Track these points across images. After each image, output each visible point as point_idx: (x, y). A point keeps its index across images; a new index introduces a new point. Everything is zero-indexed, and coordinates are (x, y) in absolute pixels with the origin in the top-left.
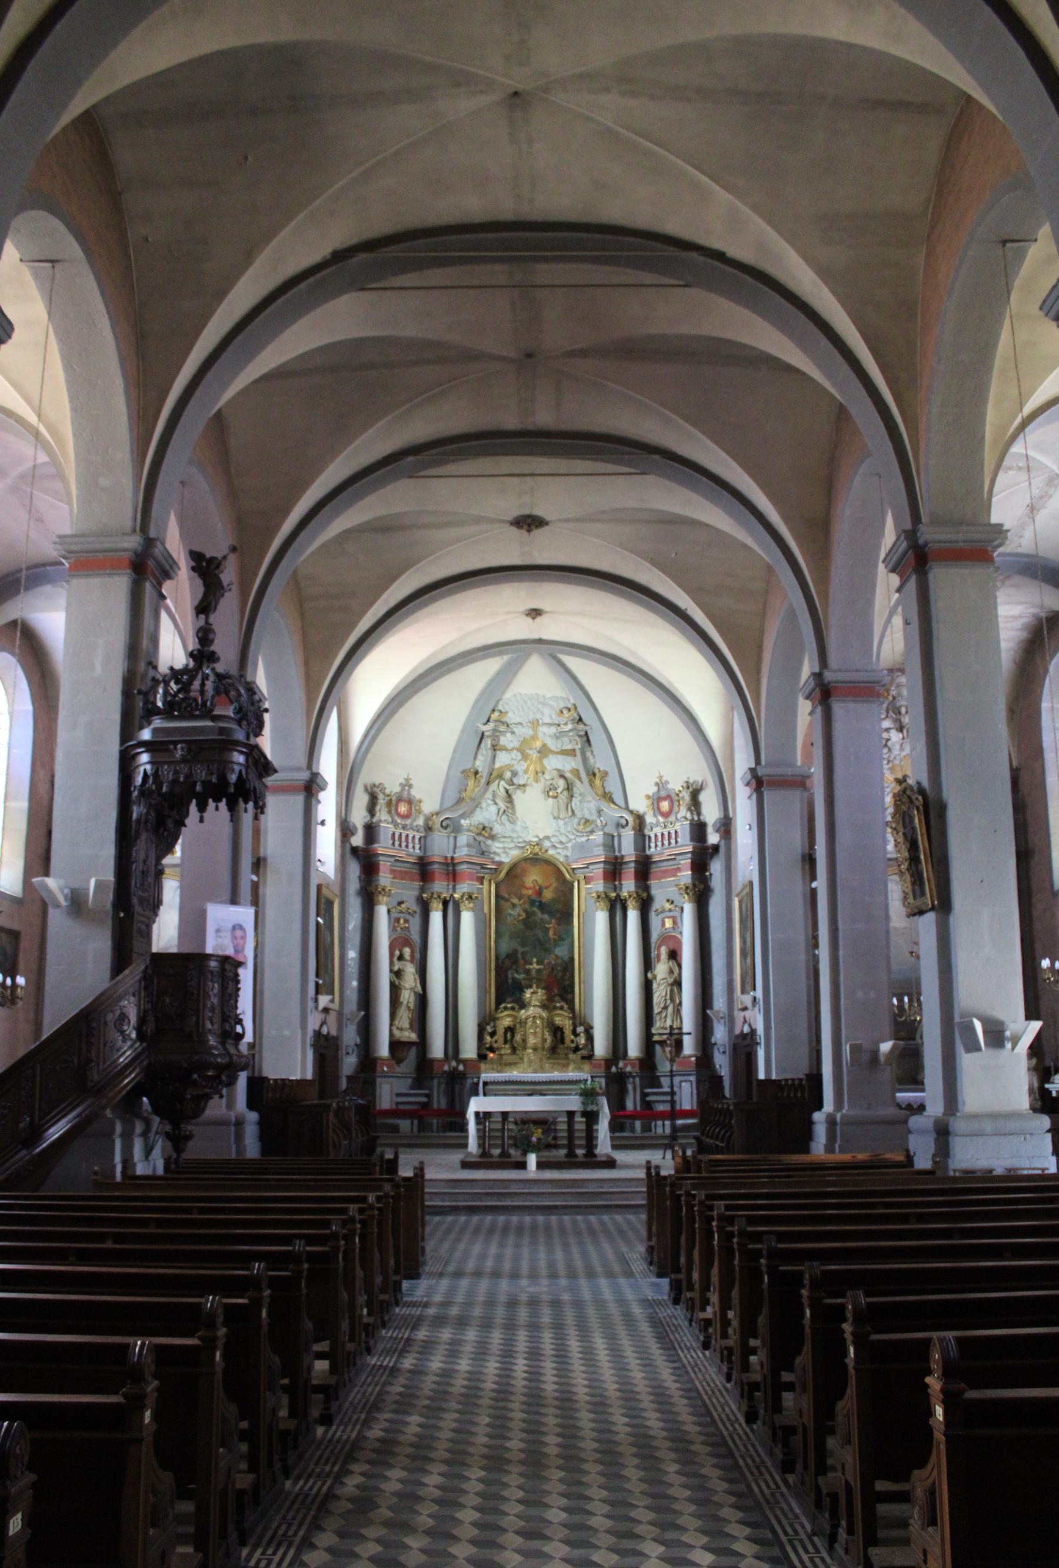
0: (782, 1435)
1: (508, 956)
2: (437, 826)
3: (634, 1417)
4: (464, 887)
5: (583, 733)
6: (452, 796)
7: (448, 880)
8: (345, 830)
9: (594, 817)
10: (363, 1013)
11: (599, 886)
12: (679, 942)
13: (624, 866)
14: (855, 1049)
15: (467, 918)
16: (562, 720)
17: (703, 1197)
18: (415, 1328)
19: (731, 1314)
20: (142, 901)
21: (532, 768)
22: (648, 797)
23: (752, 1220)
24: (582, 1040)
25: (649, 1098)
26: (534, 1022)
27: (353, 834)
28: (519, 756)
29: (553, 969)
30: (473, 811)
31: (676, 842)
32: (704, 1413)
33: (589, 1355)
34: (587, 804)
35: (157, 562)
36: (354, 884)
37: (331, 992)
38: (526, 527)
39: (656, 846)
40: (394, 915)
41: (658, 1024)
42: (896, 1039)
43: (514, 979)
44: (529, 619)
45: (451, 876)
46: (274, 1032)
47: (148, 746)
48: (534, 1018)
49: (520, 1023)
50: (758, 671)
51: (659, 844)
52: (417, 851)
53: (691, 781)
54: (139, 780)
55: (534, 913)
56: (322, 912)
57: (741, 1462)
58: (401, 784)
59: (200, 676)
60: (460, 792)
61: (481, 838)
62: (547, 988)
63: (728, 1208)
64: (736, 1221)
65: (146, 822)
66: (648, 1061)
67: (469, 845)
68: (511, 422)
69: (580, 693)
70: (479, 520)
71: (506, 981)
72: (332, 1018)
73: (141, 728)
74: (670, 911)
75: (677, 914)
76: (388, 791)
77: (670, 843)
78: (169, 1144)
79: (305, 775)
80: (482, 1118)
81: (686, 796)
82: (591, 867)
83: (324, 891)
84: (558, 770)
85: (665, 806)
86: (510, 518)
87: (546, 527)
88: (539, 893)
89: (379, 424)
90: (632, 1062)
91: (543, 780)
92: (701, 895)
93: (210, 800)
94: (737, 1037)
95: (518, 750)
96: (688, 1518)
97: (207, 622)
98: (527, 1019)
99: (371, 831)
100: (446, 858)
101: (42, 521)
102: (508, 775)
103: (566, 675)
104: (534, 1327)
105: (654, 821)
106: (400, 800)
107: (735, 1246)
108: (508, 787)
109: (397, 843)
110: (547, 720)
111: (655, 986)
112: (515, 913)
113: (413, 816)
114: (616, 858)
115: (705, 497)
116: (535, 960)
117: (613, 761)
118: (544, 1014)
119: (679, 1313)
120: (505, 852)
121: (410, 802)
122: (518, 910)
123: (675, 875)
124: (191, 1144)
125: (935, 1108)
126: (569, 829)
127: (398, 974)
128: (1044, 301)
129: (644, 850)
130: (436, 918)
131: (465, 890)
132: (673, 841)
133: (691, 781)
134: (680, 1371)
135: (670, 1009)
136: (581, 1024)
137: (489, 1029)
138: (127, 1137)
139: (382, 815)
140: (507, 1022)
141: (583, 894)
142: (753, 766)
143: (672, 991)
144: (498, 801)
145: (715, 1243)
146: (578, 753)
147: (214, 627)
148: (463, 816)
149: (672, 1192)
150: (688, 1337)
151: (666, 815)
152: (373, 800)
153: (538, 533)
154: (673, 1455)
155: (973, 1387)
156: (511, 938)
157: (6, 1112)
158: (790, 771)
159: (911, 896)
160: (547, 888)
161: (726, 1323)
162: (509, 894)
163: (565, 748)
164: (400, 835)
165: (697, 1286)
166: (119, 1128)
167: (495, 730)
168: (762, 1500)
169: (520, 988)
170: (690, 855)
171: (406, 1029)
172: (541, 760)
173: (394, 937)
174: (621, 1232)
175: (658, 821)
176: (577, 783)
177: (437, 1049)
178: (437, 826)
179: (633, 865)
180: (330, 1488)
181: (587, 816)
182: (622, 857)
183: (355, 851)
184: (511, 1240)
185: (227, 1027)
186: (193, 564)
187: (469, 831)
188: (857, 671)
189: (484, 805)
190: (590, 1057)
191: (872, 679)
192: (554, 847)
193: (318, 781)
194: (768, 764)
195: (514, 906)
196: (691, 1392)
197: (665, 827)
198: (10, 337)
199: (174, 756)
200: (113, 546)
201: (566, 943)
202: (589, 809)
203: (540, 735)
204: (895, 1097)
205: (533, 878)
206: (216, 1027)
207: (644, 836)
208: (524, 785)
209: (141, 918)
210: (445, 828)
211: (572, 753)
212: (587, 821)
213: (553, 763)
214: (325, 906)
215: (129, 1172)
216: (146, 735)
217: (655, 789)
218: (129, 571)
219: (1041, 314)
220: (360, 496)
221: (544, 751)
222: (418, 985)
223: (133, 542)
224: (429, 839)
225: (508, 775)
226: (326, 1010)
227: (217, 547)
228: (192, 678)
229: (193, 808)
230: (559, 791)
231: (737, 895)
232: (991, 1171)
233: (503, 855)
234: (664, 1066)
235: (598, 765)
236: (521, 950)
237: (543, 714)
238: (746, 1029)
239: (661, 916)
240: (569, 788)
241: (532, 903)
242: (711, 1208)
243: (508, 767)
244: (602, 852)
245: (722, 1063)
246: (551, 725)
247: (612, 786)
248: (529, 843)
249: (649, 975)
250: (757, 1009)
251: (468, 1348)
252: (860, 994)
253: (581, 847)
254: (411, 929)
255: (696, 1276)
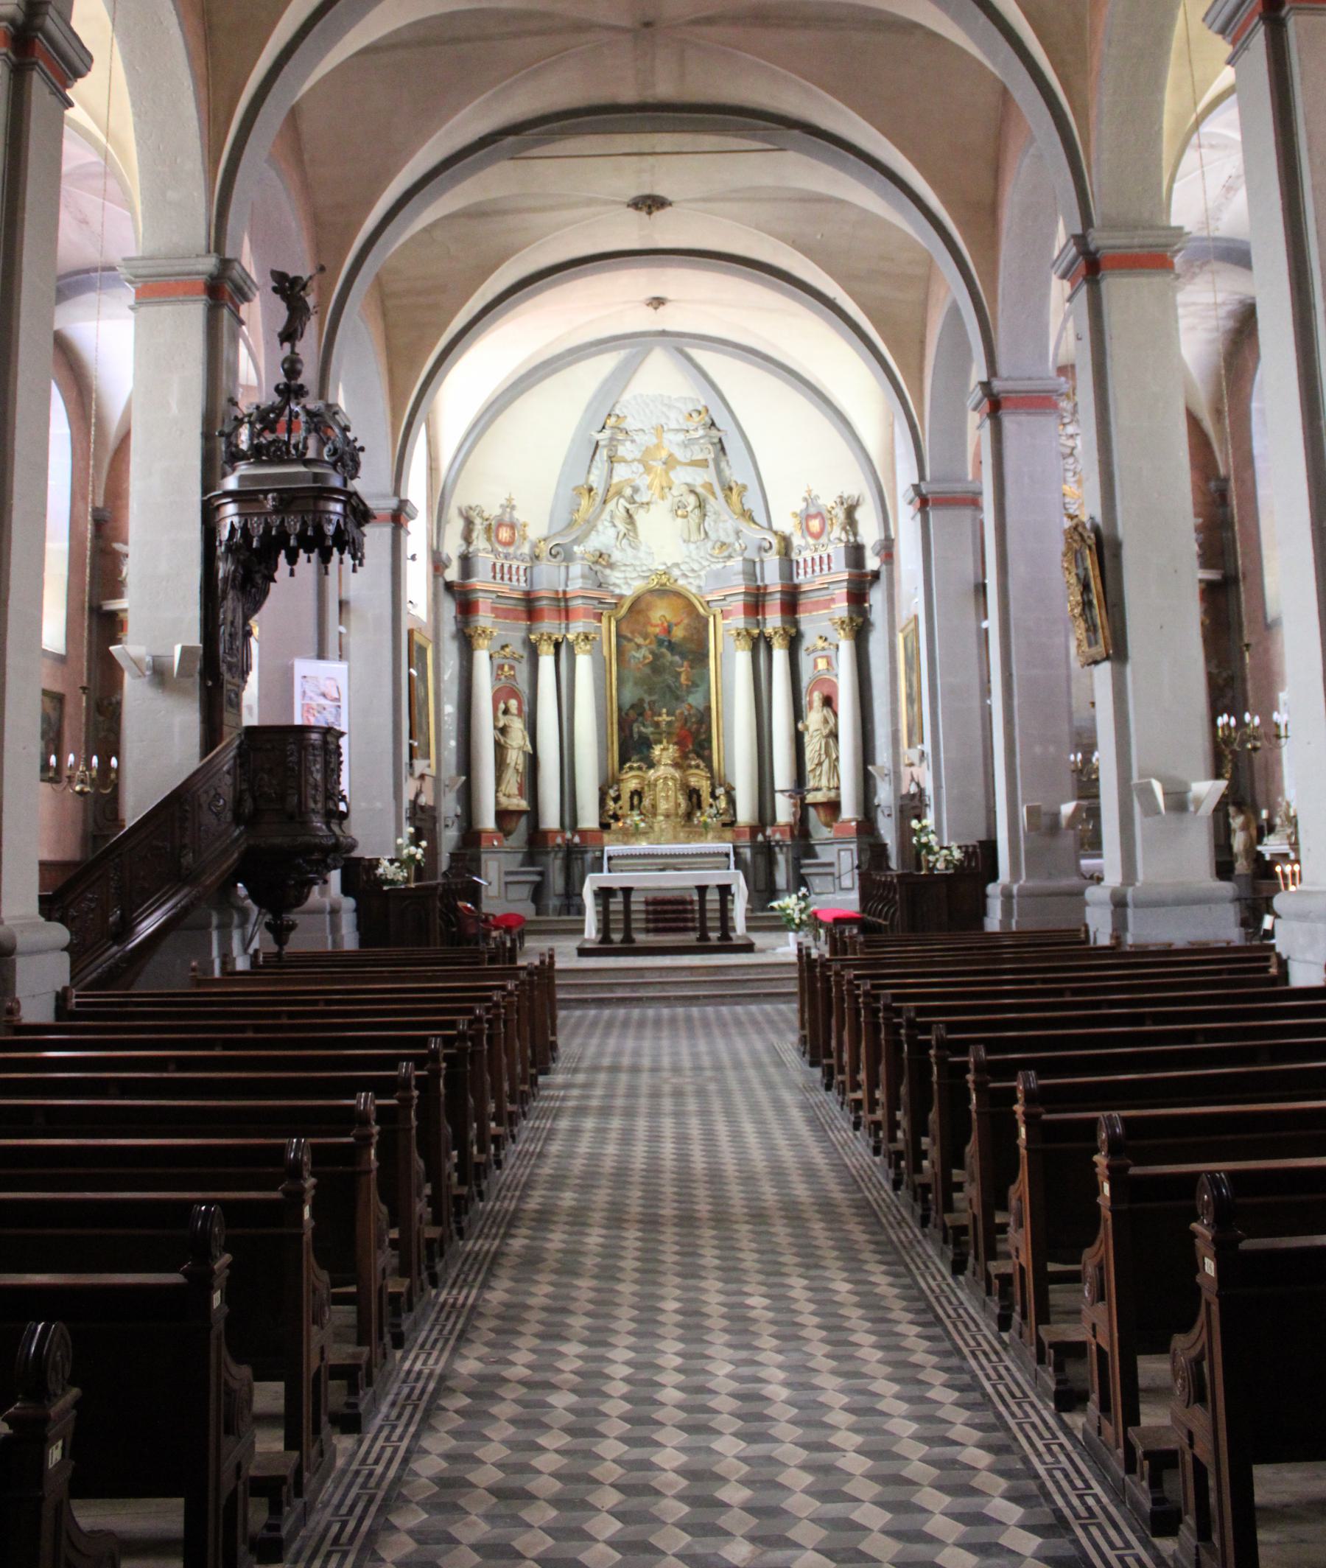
0: (921, 1192)
1: (633, 707)
2: (545, 554)
3: (778, 1174)
4: (578, 627)
5: (716, 440)
6: (563, 519)
7: (560, 618)
8: (438, 564)
9: (731, 539)
10: (463, 778)
11: (739, 621)
12: (834, 686)
13: (768, 598)
14: (1031, 811)
15: (584, 664)
16: (691, 425)
17: (868, 987)
18: (556, 1118)
19: (899, 1115)
20: (230, 668)
21: (656, 483)
22: (795, 515)
23: (951, 1027)
24: (722, 804)
25: (803, 871)
26: (665, 784)
27: (447, 567)
28: (641, 469)
29: (686, 720)
30: (586, 535)
31: (829, 568)
32: (851, 1181)
33: (736, 1136)
34: (723, 523)
35: (233, 281)
36: (449, 627)
37: (427, 756)
38: (645, 209)
39: (806, 573)
40: (497, 661)
41: (811, 783)
42: (1080, 798)
43: (640, 733)
44: (650, 309)
45: (563, 614)
46: (363, 804)
47: (235, 496)
48: (666, 778)
49: (649, 785)
50: (921, 370)
51: (809, 570)
52: (523, 584)
53: (845, 496)
54: (225, 534)
55: (662, 655)
56: (415, 661)
57: (884, 1221)
58: (502, 506)
59: (287, 412)
60: (572, 513)
61: (597, 568)
62: (680, 743)
63: (874, 987)
64: (972, 1048)
65: (234, 580)
66: (801, 829)
67: (583, 577)
68: (628, 94)
69: (713, 393)
70: (589, 202)
71: (631, 736)
72: (428, 783)
73: (224, 475)
74: (823, 649)
75: (832, 653)
76: (486, 515)
77: (821, 570)
78: (269, 936)
79: (393, 503)
80: (604, 894)
81: (840, 514)
82: (729, 599)
83: (417, 637)
84: (687, 484)
85: (815, 525)
86: (627, 200)
87: (668, 209)
88: (668, 630)
89: (476, 102)
90: (781, 829)
91: (670, 497)
92: (860, 631)
93: (301, 551)
94: (903, 797)
95: (639, 461)
96: (830, 1256)
97: (293, 352)
98: (656, 780)
99: (466, 562)
100: (557, 592)
101: (87, 223)
102: (628, 492)
103: (695, 371)
104: (679, 1115)
105: (802, 543)
106: (500, 525)
107: (881, 1021)
108: (628, 506)
109: (498, 576)
110: (674, 425)
111: (807, 739)
112: (639, 655)
113: (517, 543)
114: (758, 588)
115: (851, 174)
116: (664, 710)
117: (753, 473)
118: (677, 774)
119: (831, 1098)
120: (627, 583)
121: (512, 526)
122: (644, 651)
123: (828, 607)
124: (292, 935)
125: (1113, 878)
126: (702, 554)
127: (503, 731)
128: (1207, 14)
129: (791, 578)
130: (546, 662)
131: (581, 630)
132: (825, 567)
133: (845, 496)
134: (831, 1150)
135: (826, 765)
136: (721, 785)
137: (612, 793)
138: (224, 928)
139: (480, 542)
140: (632, 784)
141: (720, 632)
142: (916, 481)
143: (827, 744)
144: (617, 522)
145: (935, 1078)
146: (711, 464)
147: (301, 357)
148: (577, 541)
149: (822, 973)
150: (843, 1120)
151: (817, 536)
152: (469, 524)
153: (658, 214)
154: (819, 1216)
155: (1138, 1163)
156: (636, 684)
157: (93, 905)
158: (958, 487)
159: (1085, 643)
160: (676, 625)
161: (894, 1125)
162: (632, 632)
163: (695, 458)
164: (502, 566)
165: (847, 1069)
166: (215, 920)
167: (612, 439)
168: (898, 1244)
169: (646, 744)
170: (845, 584)
171: (514, 796)
172: (667, 472)
173: (499, 685)
174: (771, 1022)
175: (807, 543)
176: (711, 499)
177: (551, 818)
178: (545, 554)
179: (778, 596)
180: (499, 1247)
181: (724, 539)
182: (766, 587)
183: (449, 586)
184: (648, 1033)
185: (331, 805)
186: (275, 284)
187: (583, 559)
188: (1030, 379)
189: (600, 527)
190: (731, 824)
191: (1050, 388)
192: (685, 576)
193: (408, 509)
194: (934, 480)
195: (639, 646)
196: (840, 1168)
197: (816, 550)
198: (89, 70)
199: (264, 507)
200: (187, 269)
201: (701, 689)
202: (725, 530)
203: (666, 443)
204: (1078, 865)
205: (660, 613)
206: (320, 805)
207: (791, 561)
208: (648, 504)
209: (230, 687)
210: (555, 556)
211: (703, 464)
212: (723, 544)
213: (682, 476)
214: (417, 654)
215: (229, 968)
216: (231, 483)
217: (803, 505)
218: (204, 297)
219: (1204, 26)
220: (456, 181)
221: (670, 463)
222: (528, 743)
223: (209, 264)
224: (536, 570)
225: (628, 492)
226: (422, 777)
227: (301, 267)
228: (280, 415)
229: (282, 559)
230: (689, 509)
231: (902, 631)
232: (1170, 945)
233: (624, 587)
234: (820, 832)
235: (734, 478)
236: (647, 698)
237: (668, 418)
238: (913, 789)
239: (812, 656)
240: (701, 505)
241: (660, 643)
242: (877, 998)
243: (628, 482)
244: (741, 582)
245: (887, 830)
246: (678, 431)
247: (753, 502)
248: (655, 572)
249: (800, 726)
250: (925, 764)
251: (614, 1135)
252: (1038, 750)
253: (717, 575)
254: (518, 676)
255: (846, 1057)
